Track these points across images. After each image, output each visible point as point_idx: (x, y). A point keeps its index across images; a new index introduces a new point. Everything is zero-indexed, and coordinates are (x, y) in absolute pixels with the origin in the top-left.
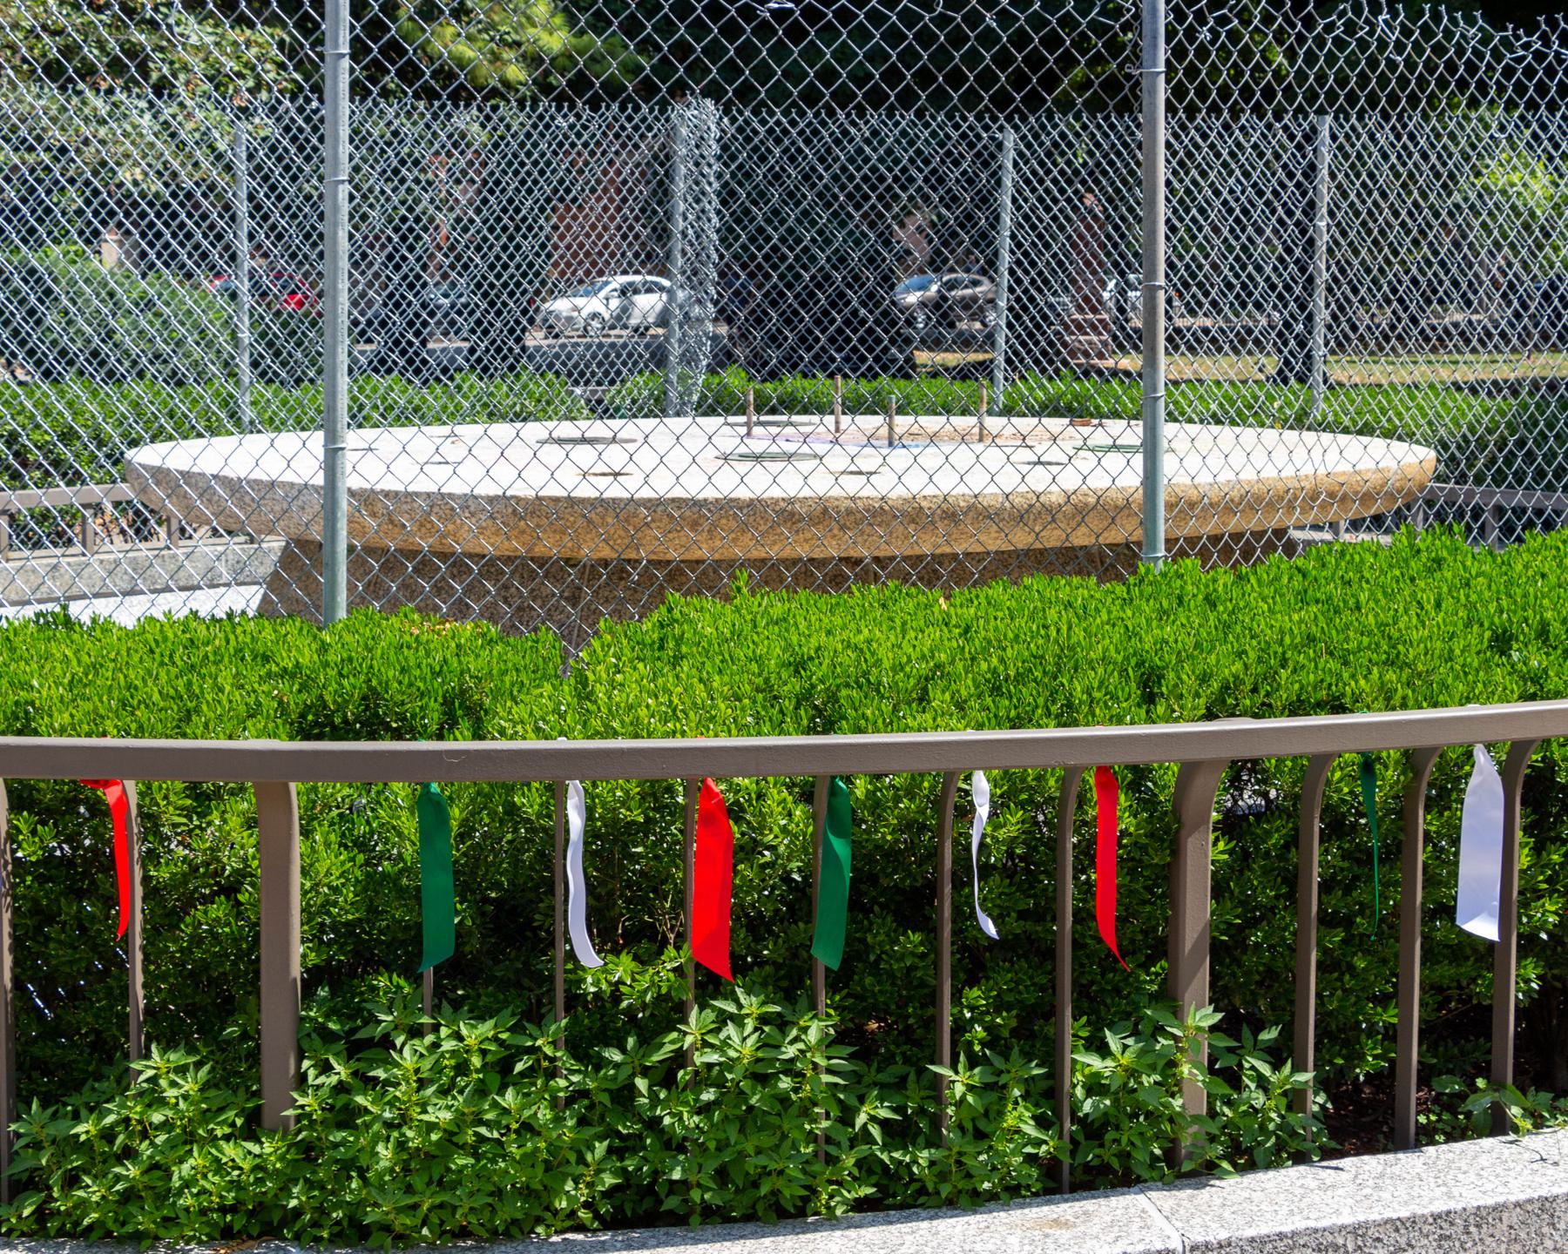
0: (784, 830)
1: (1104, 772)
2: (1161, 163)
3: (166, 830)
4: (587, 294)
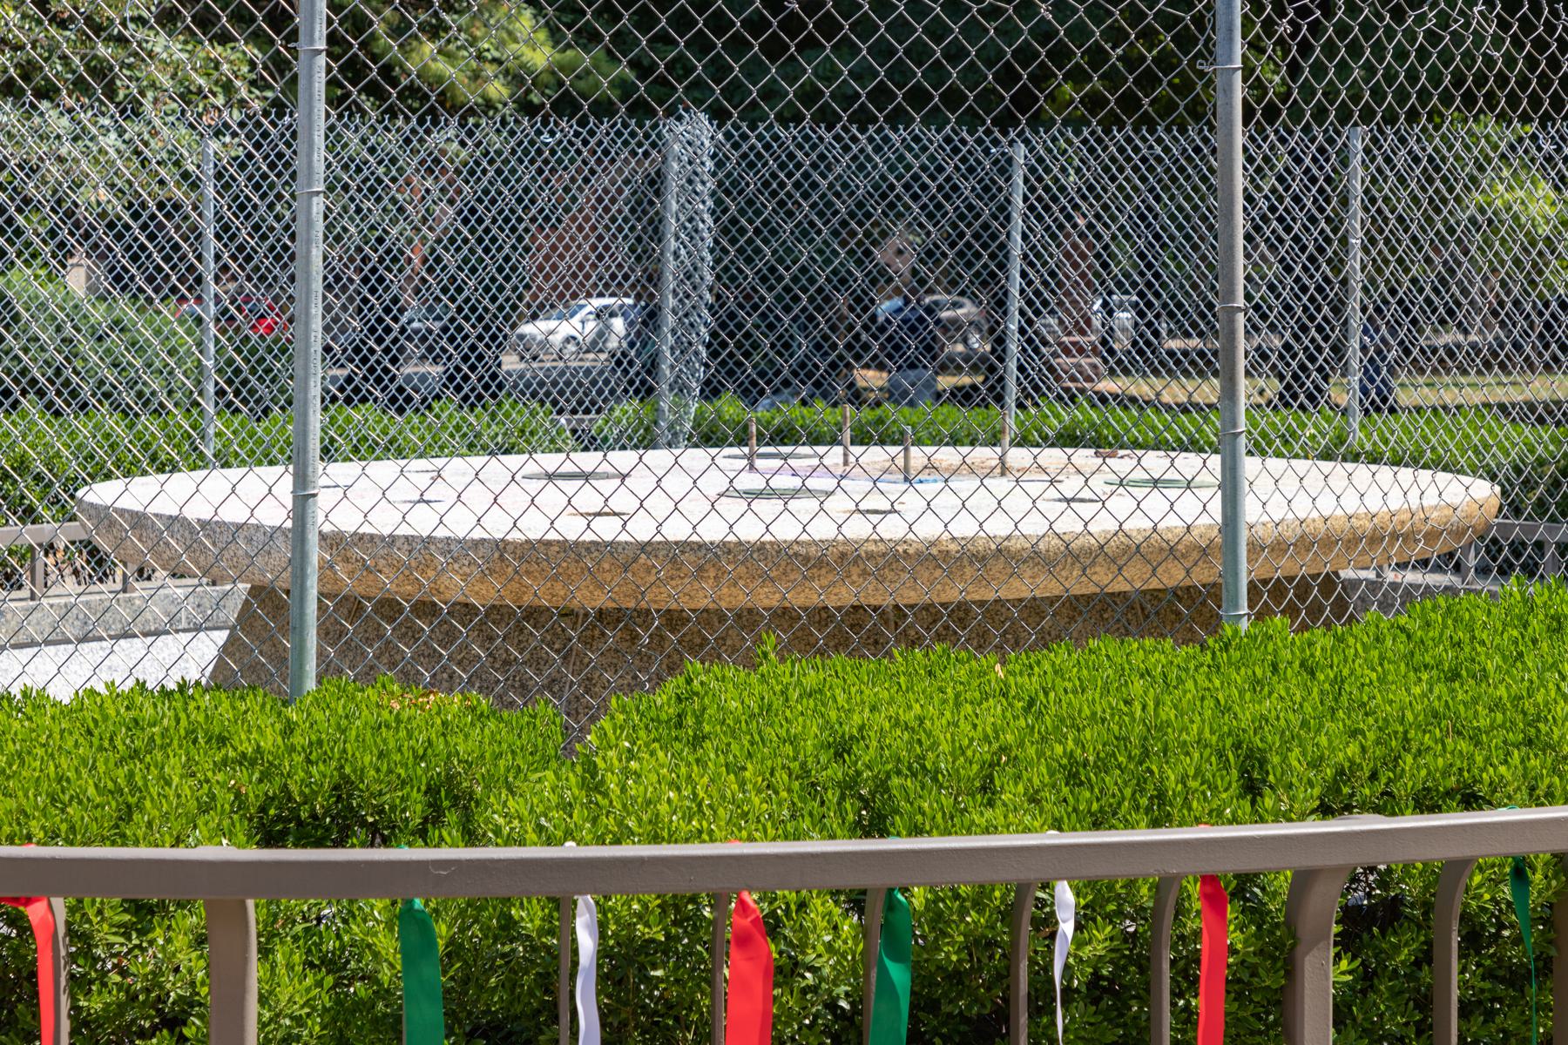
0: (829, 947)
1: (1209, 880)
2: (1239, 171)
3: (99, 952)
4: (561, 317)
